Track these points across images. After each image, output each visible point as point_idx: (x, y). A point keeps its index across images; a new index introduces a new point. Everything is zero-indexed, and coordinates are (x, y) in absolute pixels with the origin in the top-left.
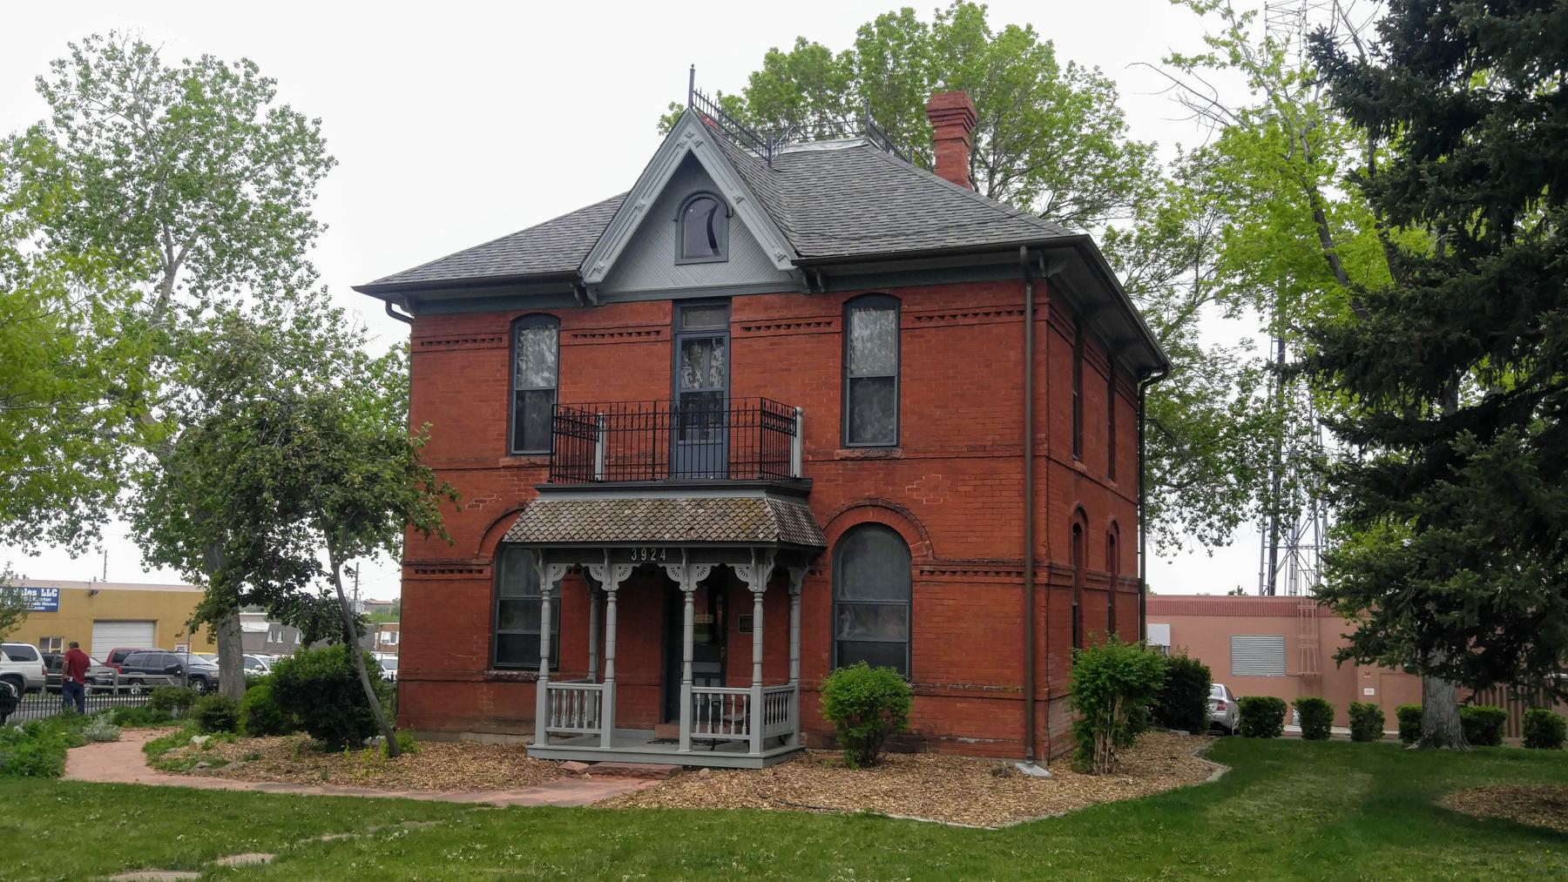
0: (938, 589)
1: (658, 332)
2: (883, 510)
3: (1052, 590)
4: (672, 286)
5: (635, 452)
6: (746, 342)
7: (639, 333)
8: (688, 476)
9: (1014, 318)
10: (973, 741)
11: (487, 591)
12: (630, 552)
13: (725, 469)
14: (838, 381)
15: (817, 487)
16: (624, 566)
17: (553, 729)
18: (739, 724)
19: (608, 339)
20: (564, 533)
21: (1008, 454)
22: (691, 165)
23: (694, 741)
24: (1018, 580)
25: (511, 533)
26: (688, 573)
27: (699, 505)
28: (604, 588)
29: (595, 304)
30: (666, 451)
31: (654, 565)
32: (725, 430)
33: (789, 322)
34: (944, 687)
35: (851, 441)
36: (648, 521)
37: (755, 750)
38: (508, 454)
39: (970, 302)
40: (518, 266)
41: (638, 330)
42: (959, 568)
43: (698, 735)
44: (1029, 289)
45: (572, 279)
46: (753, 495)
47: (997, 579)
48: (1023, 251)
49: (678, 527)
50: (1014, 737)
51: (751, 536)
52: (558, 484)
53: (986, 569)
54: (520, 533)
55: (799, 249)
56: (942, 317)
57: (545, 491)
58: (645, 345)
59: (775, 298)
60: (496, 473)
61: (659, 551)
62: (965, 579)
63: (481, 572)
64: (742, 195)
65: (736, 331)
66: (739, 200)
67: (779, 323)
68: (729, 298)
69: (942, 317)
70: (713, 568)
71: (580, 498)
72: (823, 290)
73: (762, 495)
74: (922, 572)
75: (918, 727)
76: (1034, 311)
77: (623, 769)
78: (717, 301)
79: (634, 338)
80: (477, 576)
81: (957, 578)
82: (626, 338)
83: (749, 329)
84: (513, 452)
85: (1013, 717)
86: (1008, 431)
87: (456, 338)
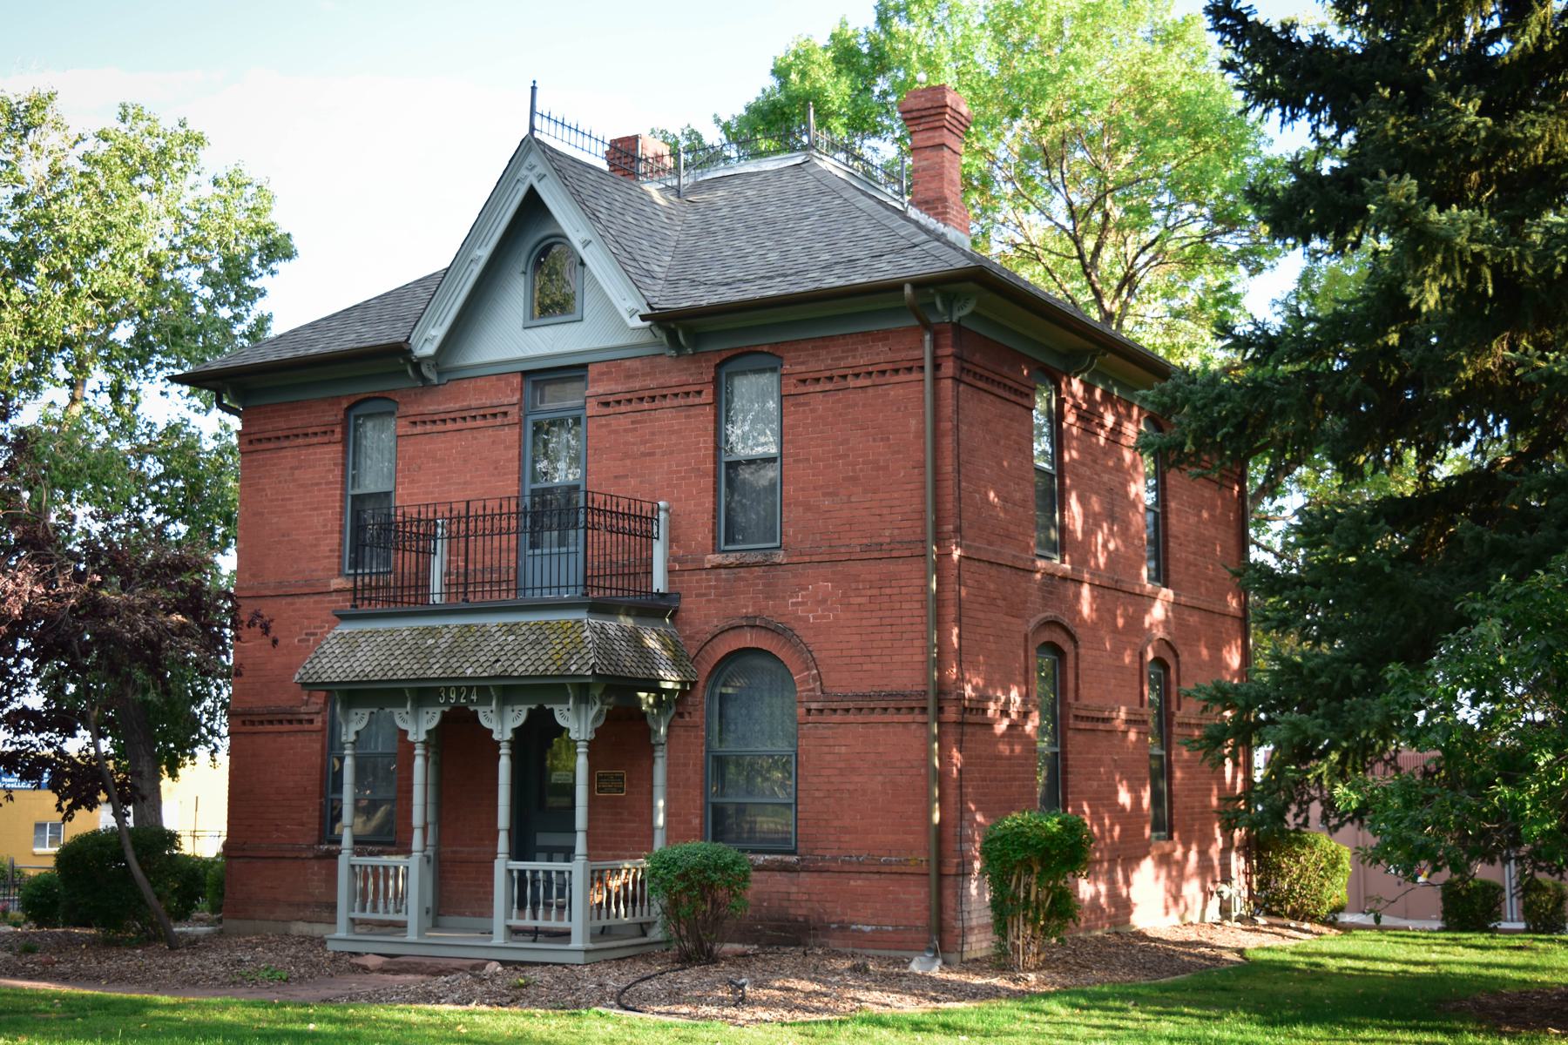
0: (828, 732)
1: (505, 414)
2: (763, 632)
3: (968, 730)
4: (519, 354)
5: (479, 566)
6: (603, 421)
7: (484, 416)
8: (537, 592)
9: (915, 376)
10: (868, 929)
11: (318, 746)
12: (435, 692)
13: (580, 581)
14: (710, 465)
15: (687, 603)
16: (431, 710)
17: (357, 915)
18: (561, 908)
19: (450, 426)
20: (358, 670)
21: (907, 553)
22: (533, 207)
23: (514, 932)
24: (920, 718)
25: (302, 671)
26: (416, 721)
27: (510, 629)
28: (411, 738)
29: (435, 381)
30: (513, 564)
31: (465, 708)
32: (581, 532)
33: (652, 393)
34: (834, 859)
35: (726, 544)
36: (451, 651)
37: (577, 942)
38: (341, 574)
39: (863, 357)
40: (347, 341)
41: (482, 412)
42: (851, 705)
43: (515, 922)
44: (927, 337)
45: (398, 353)
46: (570, 616)
47: (897, 718)
48: (908, 289)
49: (482, 659)
50: (918, 923)
51: (563, 668)
52: (365, 608)
53: (884, 705)
54: (311, 672)
55: (652, 301)
56: (830, 379)
57: (344, 617)
58: (490, 431)
59: (637, 364)
60: (328, 598)
61: (470, 689)
62: (860, 718)
63: (311, 721)
64: (589, 237)
65: (592, 408)
66: (586, 244)
67: (641, 394)
68: (584, 366)
69: (830, 379)
70: (530, 710)
71: (382, 625)
72: (690, 351)
73: (582, 615)
74: (809, 710)
75: (804, 912)
76: (937, 367)
77: (419, 964)
78: (570, 372)
79: (479, 423)
80: (306, 726)
81: (850, 717)
82: (470, 424)
83: (607, 404)
84: (723, 547)
85: (916, 897)
86: (909, 523)
87: (286, 433)
